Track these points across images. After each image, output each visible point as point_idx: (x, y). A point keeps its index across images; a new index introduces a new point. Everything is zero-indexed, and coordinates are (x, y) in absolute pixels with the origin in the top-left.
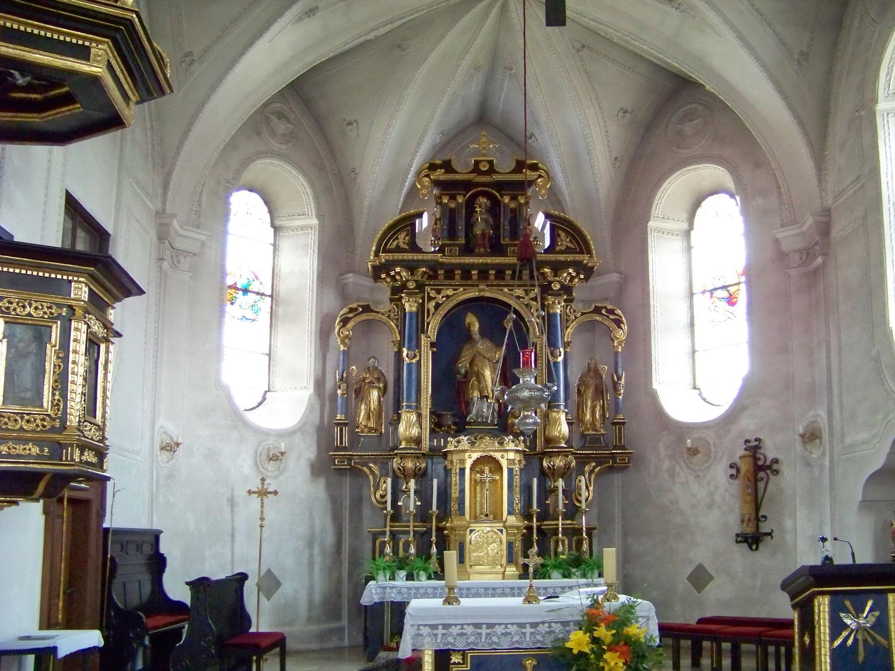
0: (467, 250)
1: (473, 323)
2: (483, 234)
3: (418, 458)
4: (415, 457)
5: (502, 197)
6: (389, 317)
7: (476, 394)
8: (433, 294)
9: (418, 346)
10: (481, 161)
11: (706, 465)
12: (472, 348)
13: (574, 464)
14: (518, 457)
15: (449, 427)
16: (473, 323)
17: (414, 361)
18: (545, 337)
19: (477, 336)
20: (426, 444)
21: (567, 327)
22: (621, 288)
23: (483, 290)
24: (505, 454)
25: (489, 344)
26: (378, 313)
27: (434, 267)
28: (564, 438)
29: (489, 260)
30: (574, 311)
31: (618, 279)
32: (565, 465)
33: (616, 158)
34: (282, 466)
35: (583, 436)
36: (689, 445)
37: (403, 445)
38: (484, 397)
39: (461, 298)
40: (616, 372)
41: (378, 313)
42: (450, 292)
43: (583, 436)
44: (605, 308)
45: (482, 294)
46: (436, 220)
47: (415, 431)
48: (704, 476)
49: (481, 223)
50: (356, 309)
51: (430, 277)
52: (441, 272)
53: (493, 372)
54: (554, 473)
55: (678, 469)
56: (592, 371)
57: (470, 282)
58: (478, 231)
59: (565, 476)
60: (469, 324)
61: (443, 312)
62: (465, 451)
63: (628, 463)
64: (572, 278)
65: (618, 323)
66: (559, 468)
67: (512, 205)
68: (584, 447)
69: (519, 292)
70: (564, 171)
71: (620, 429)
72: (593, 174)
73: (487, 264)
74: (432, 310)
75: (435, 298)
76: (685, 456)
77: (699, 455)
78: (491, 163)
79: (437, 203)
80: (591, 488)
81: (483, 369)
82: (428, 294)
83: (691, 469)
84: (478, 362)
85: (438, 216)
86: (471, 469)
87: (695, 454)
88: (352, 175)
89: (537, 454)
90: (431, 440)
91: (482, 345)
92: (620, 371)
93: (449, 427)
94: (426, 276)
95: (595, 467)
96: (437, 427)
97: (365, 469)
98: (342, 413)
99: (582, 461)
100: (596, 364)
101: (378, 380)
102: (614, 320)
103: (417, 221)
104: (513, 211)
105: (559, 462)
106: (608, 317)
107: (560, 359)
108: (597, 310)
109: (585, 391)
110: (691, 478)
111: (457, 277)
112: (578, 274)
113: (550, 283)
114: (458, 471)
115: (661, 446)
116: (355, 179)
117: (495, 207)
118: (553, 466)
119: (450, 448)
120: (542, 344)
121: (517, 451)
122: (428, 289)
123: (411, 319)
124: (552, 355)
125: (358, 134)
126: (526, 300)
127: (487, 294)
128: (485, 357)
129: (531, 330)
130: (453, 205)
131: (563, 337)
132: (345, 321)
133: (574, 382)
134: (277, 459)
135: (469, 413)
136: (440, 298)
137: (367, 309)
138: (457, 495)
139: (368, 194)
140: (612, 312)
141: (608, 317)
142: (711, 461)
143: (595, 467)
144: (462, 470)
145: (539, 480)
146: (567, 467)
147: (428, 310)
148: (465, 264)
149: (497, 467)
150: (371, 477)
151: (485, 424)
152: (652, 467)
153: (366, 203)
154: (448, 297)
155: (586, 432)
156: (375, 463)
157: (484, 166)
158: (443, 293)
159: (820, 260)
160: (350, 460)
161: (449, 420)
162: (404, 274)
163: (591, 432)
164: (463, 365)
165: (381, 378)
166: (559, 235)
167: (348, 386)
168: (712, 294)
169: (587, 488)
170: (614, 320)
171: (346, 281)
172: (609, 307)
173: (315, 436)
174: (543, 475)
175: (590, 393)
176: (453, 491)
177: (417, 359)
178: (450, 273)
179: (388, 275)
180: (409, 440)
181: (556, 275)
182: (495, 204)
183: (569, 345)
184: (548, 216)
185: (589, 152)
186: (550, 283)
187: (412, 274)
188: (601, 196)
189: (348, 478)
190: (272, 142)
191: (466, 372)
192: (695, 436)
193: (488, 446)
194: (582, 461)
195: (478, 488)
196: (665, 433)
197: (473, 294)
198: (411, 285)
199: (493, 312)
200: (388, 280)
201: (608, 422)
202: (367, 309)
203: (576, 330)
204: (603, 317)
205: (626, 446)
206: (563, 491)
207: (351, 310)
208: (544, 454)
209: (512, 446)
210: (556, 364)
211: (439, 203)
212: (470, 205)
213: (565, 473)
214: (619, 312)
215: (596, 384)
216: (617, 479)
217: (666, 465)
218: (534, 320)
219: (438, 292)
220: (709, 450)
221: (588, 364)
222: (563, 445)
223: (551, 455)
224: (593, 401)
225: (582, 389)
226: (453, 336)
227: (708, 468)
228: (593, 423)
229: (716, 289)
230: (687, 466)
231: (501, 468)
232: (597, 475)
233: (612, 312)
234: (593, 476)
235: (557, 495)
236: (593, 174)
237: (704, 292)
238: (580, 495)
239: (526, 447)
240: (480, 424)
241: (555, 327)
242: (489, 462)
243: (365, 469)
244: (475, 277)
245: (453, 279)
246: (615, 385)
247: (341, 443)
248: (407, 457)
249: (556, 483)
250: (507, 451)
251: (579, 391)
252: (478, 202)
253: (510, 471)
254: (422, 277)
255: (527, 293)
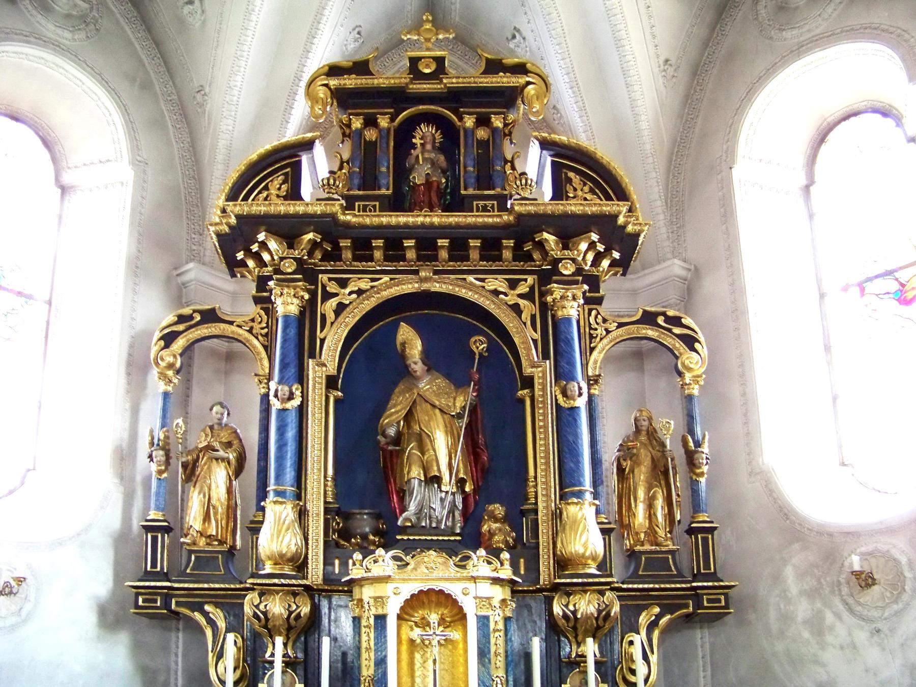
0: (396, 204)
1: (411, 342)
2: (428, 184)
3: (295, 594)
4: (288, 593)
5: (461, 119)
6: (250, 331)
7: (416, 473)
8: (332, 288)
9: (301, 378)
10: (420, 59)
11: (895, 607)
12: (410, 390)
13: (616, 609)
14: (499, 593)
15: (364, 537)
16: (411, 342)
17: (289, 405)
18: (549, 365)
19: (418, 367)
20: (316, 573)
21: (592, 350)
22: (689, 290)
23: (426, 280)
24: (471, 585)
25: (441, 382)
26: (231, 323)
27: (329, 229)
28: (594, 559)
29: (437, 218)
30: (605, 321)
31: (683, 273)
32: (599, 612)
33: (667, 61)
34: (28, 607)
35: (632, 555)
36: (857, 568)
37: (268, 568)
38: (434, 480)
39: (386, 294)
40: (691, 432)
41: (231, 323)
42: (364, 285)
43: (632, 555)
44: (664, 314)
45: (426, 286)
46: (342, 162)
47: (290, 543)
48: (892, 630)
49: (423, 169)
50: (190, 317)
51: (326, 257)
52: (345, 243)
53: (450, 431)
54: (575, 627)
55: (829, 617)
56: (645, 432)
57: (402, 266)
58: (418, 178)
59: (599, 633)
60: (403, 344)
61: (350, 319)
62: (386, 579)
63: (727, 607)
64: (598, 257)
65: (690, 341)
66: (588, 617)
67: (482, 133)
68: (635, 577)
69: (497, 283)
70: (574, 86)
71: (705, 540)
72: (627, 85)
73: (432, 226)
74: (331, 316)
75: (336, 295)
76: (845, 590)
77: (876, 588)
78: (440, 61)
79: (344, 135)
80: (654, 659)
81: (428, 425)
82: (324, 287)
83: (861, 617)
84: (421, 414)
85: (346, 156)
86: (399, 617)
87: (868, 586)
88: (199, 96)
89: (540, 590)
90: (327, 562)
91: (429, 385)
92: (698, 431)
93: (364, 537)
94: (318, 255)
95: (659, 617)
96: (342, 538)
97: (198, 616)
98: (158, 508)
99: (633, 604)
100: (650, 419)
101: (229, 445)
102: (681, 337)
103: (305, 159)
104: (483, 144)
105: (586, 605)
106: (670, 330)
107: (581, 402)
108: (649, 318)
109: (632, 471)
110: (861, 636)
111: (378, 254)
112: (608, 250)
113: (556, 262)
114: (372, 620)
115: (789, 573)
116: (201, 105)
117: (451, 138)
118: (574, 613)
119: (356, 573)
120: (544, 377)
121: (496, 581)
122: (324, 278)
123: (285, 328)
124: (564, 393)
125: (204, 22)
126: (512, 299)
127: (437, 287)
128: (434, 406)
129: (522, 352)
130: (371, 135)
131: (585, 366)
132: (169, 339)
133: (609, 455)
134: (11, 593)
135: (404, 509)
136: (345, 295)
137: (210, 316)
138: (371, 671)
139: (224, 128)
140: (676, 321)
141: (670, 330)
142: (905, 597)
143: (659, 617)
144: (381, 620)
145: (546, 640)
146: (604, 615)
147: (323, 317)
148: (388, 227)
149: (457, 615)
150: (209, 632)
151: (437, 531)
152: (773, 615)
153: (222, 144)
154: (360, 292)
155: (638, 548)
156: (217, 605)
157: (427, 66)
158: (352, 287)
159: (479, 345)
160: (167, 599)
161: (364, 523)
162: (273, 245)
163: (647, 547)
164: (392, 420)
165: (234, 441)
166: (570, 181)
167: (168, 457)
168: (862, 290)
169: (645, 658)
170: (681, 337)
171: (185, 278)
172: (671, 313)
173: (110, 554)
174: (555, 631)
175: (641, 475)
176: (364, 663)
177: (296, 402)
178: (362, 245)
179: (248, 251)
180: (280, 559)
181: (566, 247)
182: (451, 138)
183: (596, 382)
184: (545, 145)
185: (618, 44)
186: (556, 262)
187: (291, 246)
188: (644, 125)
189: (181, 635)
190: (43, 22)
191: (399, 434)
192: (863, 549)
193: (432, 570)
194: (633, 604)
195: (418, 656)
196: (796, 546)
197: (409, 286)
198: (289, 267)
199: (451, 325)
200: (251, 263)
201: (679, 530)
202: (210, 316)
203: (607, 359)
204: (661, 337)
205: (719, 575)
206: (597, 663)
207: (182, 319)
208: (555, 588)
209: (485, 570)
210: (574, 410)
211: (347, 132)
212: (403, 137)
213: (599, 627)
214: (687, 321)
215: (663, 460)
216: (701, 639)
217: (803, 609)
218: (525, 337)
219: (343, 284)
220: (900, 575)
221: (636, 419)
222: (594, 571)
223: (567, 590)
224: (649, 488)
225: (627, 465)
226: (371, 368)
227: (897, 614)
228: (651, 531)
229: (870, 279)
230: (851, 611)
231: (464, 617)
232: (663, 633)
233: (676, 321)
234: (656, 634)
235: (585, 672)
236: (627, 85)
237: (845, 289)
238: (633, 672)
239: (516, 572)
240: (424, 530)
241: (569, 343)
242: (439, 604)
243: (198, 616)
244: (411, 255)
245: (371, 259)
246: (691, 459)
247: (154, 565)
248: (271, 593)
249: (582, 648)
250: (474, 579)
251: (621, 471)
252: (418, 134)
253: (483, 621)
254: (310, 254)
255: (513, 284)
